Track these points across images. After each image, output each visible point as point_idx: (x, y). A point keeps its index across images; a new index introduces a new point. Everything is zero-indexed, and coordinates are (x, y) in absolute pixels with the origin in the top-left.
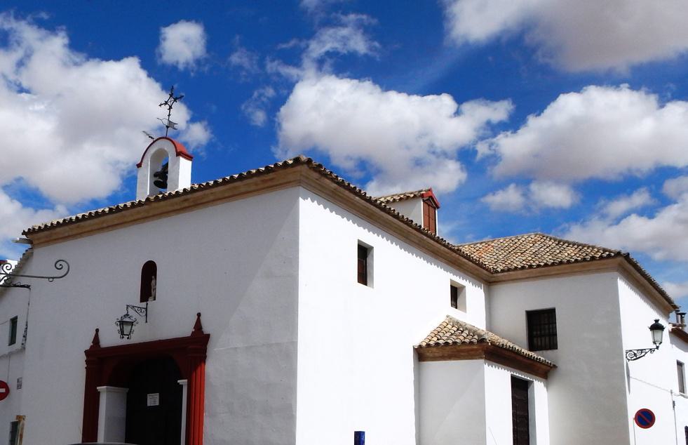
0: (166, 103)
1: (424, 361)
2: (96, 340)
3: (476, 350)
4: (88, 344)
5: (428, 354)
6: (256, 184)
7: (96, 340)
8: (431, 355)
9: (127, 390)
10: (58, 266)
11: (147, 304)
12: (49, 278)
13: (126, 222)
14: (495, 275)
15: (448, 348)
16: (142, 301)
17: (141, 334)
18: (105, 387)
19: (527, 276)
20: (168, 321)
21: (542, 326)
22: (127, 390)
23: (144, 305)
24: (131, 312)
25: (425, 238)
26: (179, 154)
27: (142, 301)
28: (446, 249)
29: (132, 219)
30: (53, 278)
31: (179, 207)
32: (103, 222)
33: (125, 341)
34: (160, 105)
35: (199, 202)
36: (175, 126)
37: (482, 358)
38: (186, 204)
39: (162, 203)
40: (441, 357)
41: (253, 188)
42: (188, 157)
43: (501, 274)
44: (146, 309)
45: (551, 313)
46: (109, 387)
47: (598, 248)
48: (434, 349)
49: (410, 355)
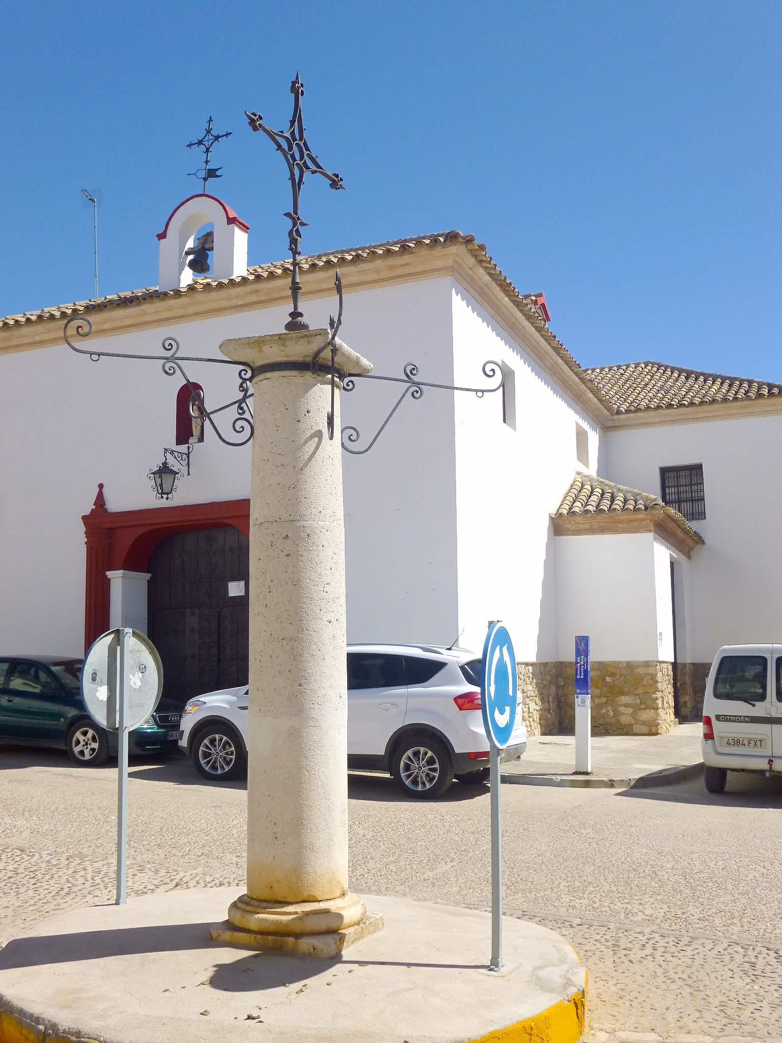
0: (217, 138)
1: (562, 534)
2: (100, 501)
3: (643, 520)
4: (88, 507)
5: (568, 526)
6: (378, 272)
7: (100, 501)
8: (573, 528)
9: (148, 576)
10: (488, 368)
11: (189, 448)
12: (477, 391)
13: (147, 323)
14: (616, 417)
15: (599, 517)
16: (179, 442)
17: (189, 492)
18: (122, 571)
19: (662, 419)
20: (217, 474)
21: (683, 486)
22: (148, 576)
23: (183, 448)
24: (171, 461)
25: (560, 361)
26: (231, 221)
27: (179, 442)
28: (576, 379)
29: (156, 317)
30: (483, 391)
31: (240, 303)
32: (105, 322)
33: (163, 503)
34: (189, 146)
35: (276, 295)
36: (218, 173)
37: (650, 531)
38: (254, 298)
39: (214, 295)
40: (587, 529)
41: (372, 276)
42: (245, 228)
43: (626, 416)
44: (188, 455)
45: (696, 469)
46: (127, 572)
47: (758, 383)
48: (579, 519)
49: (544, 525)
